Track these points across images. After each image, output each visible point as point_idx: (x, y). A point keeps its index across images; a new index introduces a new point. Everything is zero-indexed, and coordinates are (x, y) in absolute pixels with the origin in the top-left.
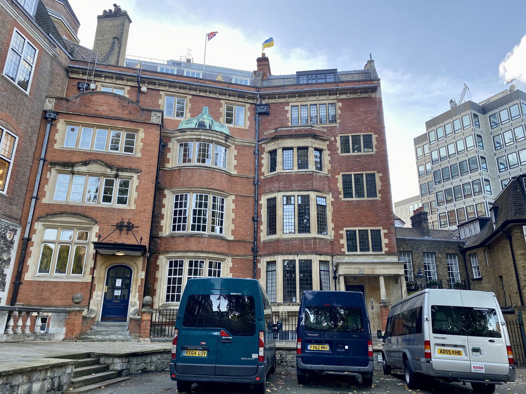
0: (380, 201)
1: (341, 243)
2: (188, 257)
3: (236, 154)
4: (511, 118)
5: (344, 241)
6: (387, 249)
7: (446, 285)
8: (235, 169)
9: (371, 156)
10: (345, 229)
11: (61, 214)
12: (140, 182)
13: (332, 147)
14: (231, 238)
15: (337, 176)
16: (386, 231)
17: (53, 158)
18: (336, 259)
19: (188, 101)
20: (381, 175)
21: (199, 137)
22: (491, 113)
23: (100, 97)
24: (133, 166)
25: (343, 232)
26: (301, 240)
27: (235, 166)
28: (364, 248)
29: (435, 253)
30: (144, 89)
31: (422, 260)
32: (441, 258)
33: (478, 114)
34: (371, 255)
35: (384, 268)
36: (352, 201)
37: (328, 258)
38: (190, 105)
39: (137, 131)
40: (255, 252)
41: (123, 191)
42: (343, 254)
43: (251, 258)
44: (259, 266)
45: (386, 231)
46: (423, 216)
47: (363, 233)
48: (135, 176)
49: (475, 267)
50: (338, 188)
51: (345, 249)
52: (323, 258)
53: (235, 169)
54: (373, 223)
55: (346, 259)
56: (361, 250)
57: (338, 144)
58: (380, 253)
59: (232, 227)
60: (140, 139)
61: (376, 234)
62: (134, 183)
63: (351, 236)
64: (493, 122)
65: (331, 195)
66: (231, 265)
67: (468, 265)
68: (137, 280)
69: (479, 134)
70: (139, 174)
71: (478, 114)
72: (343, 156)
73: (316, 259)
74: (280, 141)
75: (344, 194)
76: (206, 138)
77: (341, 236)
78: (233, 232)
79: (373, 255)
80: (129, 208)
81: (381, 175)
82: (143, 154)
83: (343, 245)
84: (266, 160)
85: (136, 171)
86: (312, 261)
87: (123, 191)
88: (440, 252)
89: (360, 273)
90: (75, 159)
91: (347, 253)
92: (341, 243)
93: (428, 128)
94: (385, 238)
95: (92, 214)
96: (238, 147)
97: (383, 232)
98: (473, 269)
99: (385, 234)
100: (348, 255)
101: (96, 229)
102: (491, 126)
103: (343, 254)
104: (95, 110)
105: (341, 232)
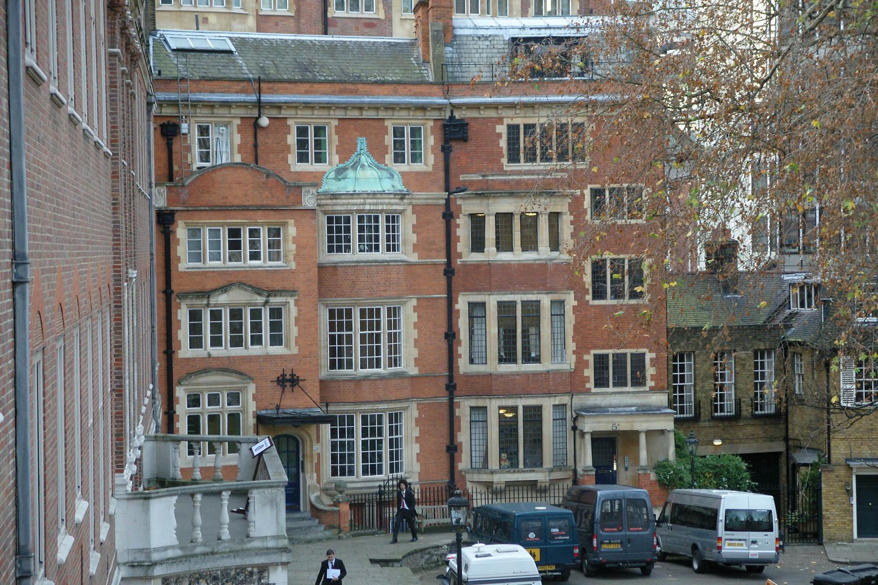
2: (361, 411)
3: (415, 223)
5: (589, 373)
6: (653, 384)
8: (414, 251)
10: (593, 352)
11: (206, 371)
12: (299, 310)
13: (576, 205)
14: (414, 371)
16: (654, 355)
17: (181, 288)
18: (579, 401)
19: (333, 130)
21: (361, 207)
23: (225, 172)
24: (287, 285)
25: (589, 358)
26: (526, 375)
27: (414, 245)
28: (620, 382)
30: (264, 121)
32: (745, 360)
34: (628, 393)
36: (604, 306)
37: (566, 400)
38: (335, 138)
39: (285, 224)
40: (451, 388)
41: (276, 327)
43: (445, 400)
44: (457, 412)
45: (654, 355)
46: (729, 251)
47: (620, 360)
48: (292, 301)
49: (799, 375)
51: (590, 385)
52: (557, 401)
53: (414, 251)
55: (591, 401)
56: (615, 385)
57: (587, 203)
58: (642, 389)
59: (415, 353)
60: (290, 238)
61: (639, 361)
62: (291, 312)
63: (601, 362)
65: (572, 295)
66: (416, 414)
68: (312, 456)
70: (296, 298)
73: (548, 404)
74: (491, 201)
75: (594, 292)
76: (372, 207)
77: (586, 363)
78: (417, 362)
79: (634, 393)
80: (290, 353)
82: (298, 264)
83: (500, 135)
84: (463, 230)
85: (292, 292)
86: (544, 407)
87: (276, 327)
90: (209, 286)
91: (594, 390)
95: (244, 368)
96: (417, 208)
98: (797, 377)
99: (651, 360)
100: (595, 394)
101: (252, 388)
103: (588, 392)
104: (223, 198)
105: (586, 357)
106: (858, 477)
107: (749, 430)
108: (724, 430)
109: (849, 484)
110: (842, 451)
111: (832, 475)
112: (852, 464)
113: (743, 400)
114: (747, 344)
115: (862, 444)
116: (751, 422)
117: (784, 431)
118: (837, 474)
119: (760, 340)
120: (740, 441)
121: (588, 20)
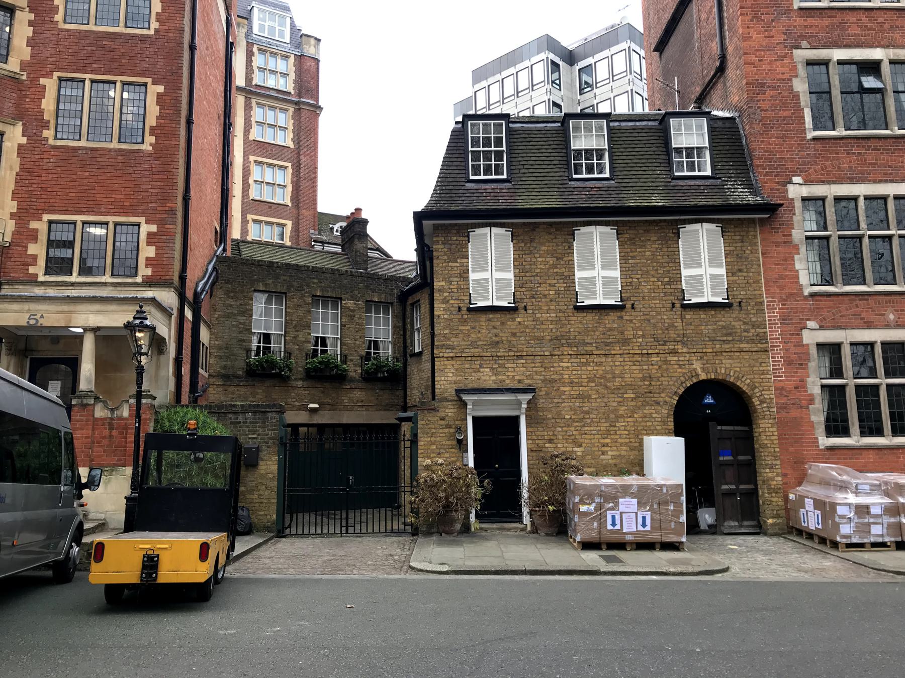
0: (149, 154)
1: (29, 252)
4: (612, 77)
5: (37, 249)
6: (149, 272)
7: (355, 365)
9: (142, 38)
10: (46, 217)
15: (42, 81)
16: (153, 228)
20: (161, 89)
22: (582, 64)
25: (40, 226)
29: (341, 299)
31: (309, 312)
32: (353, 311)
33: (561, 63)
35: (99, 312)
42: (33, 281)
45: (153, 228)
46: (357, 228)
50: (42, 112)
51: (38, 270)
54: (123, 207)
58: (129, 280)
64: (586, 83)
65: (19, 128)
67: (408, 326)
69: (559, 102)
71: (561, 63)
72: (68, 30)
77: (34, 236)
79: (112, 284)
81: (161, 89)
88: (353, 298)
89: (32, 322)
92: (29, 252)
93: (475, 81)
94: (149, 243)
97: (145, 229)
99: (149, 235)
100: (43, 284)
102: (581, 90)
105: (34, 225)
106: (474, 418)
107: (358, 394)
108: (323, 392)
109: (462, 430)
110: (451, 377)
111: (433, 418)
112: (465, 397)
113: (350, 358)
114: (356, 293)
115: (481, 366)
116: (360, 385)
117: (402, 399)
118: (443, 415)
119: (373, 291)
120: (346, 408)
121: (284, 129)
